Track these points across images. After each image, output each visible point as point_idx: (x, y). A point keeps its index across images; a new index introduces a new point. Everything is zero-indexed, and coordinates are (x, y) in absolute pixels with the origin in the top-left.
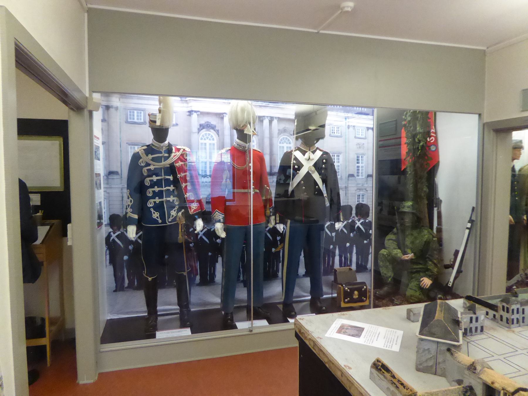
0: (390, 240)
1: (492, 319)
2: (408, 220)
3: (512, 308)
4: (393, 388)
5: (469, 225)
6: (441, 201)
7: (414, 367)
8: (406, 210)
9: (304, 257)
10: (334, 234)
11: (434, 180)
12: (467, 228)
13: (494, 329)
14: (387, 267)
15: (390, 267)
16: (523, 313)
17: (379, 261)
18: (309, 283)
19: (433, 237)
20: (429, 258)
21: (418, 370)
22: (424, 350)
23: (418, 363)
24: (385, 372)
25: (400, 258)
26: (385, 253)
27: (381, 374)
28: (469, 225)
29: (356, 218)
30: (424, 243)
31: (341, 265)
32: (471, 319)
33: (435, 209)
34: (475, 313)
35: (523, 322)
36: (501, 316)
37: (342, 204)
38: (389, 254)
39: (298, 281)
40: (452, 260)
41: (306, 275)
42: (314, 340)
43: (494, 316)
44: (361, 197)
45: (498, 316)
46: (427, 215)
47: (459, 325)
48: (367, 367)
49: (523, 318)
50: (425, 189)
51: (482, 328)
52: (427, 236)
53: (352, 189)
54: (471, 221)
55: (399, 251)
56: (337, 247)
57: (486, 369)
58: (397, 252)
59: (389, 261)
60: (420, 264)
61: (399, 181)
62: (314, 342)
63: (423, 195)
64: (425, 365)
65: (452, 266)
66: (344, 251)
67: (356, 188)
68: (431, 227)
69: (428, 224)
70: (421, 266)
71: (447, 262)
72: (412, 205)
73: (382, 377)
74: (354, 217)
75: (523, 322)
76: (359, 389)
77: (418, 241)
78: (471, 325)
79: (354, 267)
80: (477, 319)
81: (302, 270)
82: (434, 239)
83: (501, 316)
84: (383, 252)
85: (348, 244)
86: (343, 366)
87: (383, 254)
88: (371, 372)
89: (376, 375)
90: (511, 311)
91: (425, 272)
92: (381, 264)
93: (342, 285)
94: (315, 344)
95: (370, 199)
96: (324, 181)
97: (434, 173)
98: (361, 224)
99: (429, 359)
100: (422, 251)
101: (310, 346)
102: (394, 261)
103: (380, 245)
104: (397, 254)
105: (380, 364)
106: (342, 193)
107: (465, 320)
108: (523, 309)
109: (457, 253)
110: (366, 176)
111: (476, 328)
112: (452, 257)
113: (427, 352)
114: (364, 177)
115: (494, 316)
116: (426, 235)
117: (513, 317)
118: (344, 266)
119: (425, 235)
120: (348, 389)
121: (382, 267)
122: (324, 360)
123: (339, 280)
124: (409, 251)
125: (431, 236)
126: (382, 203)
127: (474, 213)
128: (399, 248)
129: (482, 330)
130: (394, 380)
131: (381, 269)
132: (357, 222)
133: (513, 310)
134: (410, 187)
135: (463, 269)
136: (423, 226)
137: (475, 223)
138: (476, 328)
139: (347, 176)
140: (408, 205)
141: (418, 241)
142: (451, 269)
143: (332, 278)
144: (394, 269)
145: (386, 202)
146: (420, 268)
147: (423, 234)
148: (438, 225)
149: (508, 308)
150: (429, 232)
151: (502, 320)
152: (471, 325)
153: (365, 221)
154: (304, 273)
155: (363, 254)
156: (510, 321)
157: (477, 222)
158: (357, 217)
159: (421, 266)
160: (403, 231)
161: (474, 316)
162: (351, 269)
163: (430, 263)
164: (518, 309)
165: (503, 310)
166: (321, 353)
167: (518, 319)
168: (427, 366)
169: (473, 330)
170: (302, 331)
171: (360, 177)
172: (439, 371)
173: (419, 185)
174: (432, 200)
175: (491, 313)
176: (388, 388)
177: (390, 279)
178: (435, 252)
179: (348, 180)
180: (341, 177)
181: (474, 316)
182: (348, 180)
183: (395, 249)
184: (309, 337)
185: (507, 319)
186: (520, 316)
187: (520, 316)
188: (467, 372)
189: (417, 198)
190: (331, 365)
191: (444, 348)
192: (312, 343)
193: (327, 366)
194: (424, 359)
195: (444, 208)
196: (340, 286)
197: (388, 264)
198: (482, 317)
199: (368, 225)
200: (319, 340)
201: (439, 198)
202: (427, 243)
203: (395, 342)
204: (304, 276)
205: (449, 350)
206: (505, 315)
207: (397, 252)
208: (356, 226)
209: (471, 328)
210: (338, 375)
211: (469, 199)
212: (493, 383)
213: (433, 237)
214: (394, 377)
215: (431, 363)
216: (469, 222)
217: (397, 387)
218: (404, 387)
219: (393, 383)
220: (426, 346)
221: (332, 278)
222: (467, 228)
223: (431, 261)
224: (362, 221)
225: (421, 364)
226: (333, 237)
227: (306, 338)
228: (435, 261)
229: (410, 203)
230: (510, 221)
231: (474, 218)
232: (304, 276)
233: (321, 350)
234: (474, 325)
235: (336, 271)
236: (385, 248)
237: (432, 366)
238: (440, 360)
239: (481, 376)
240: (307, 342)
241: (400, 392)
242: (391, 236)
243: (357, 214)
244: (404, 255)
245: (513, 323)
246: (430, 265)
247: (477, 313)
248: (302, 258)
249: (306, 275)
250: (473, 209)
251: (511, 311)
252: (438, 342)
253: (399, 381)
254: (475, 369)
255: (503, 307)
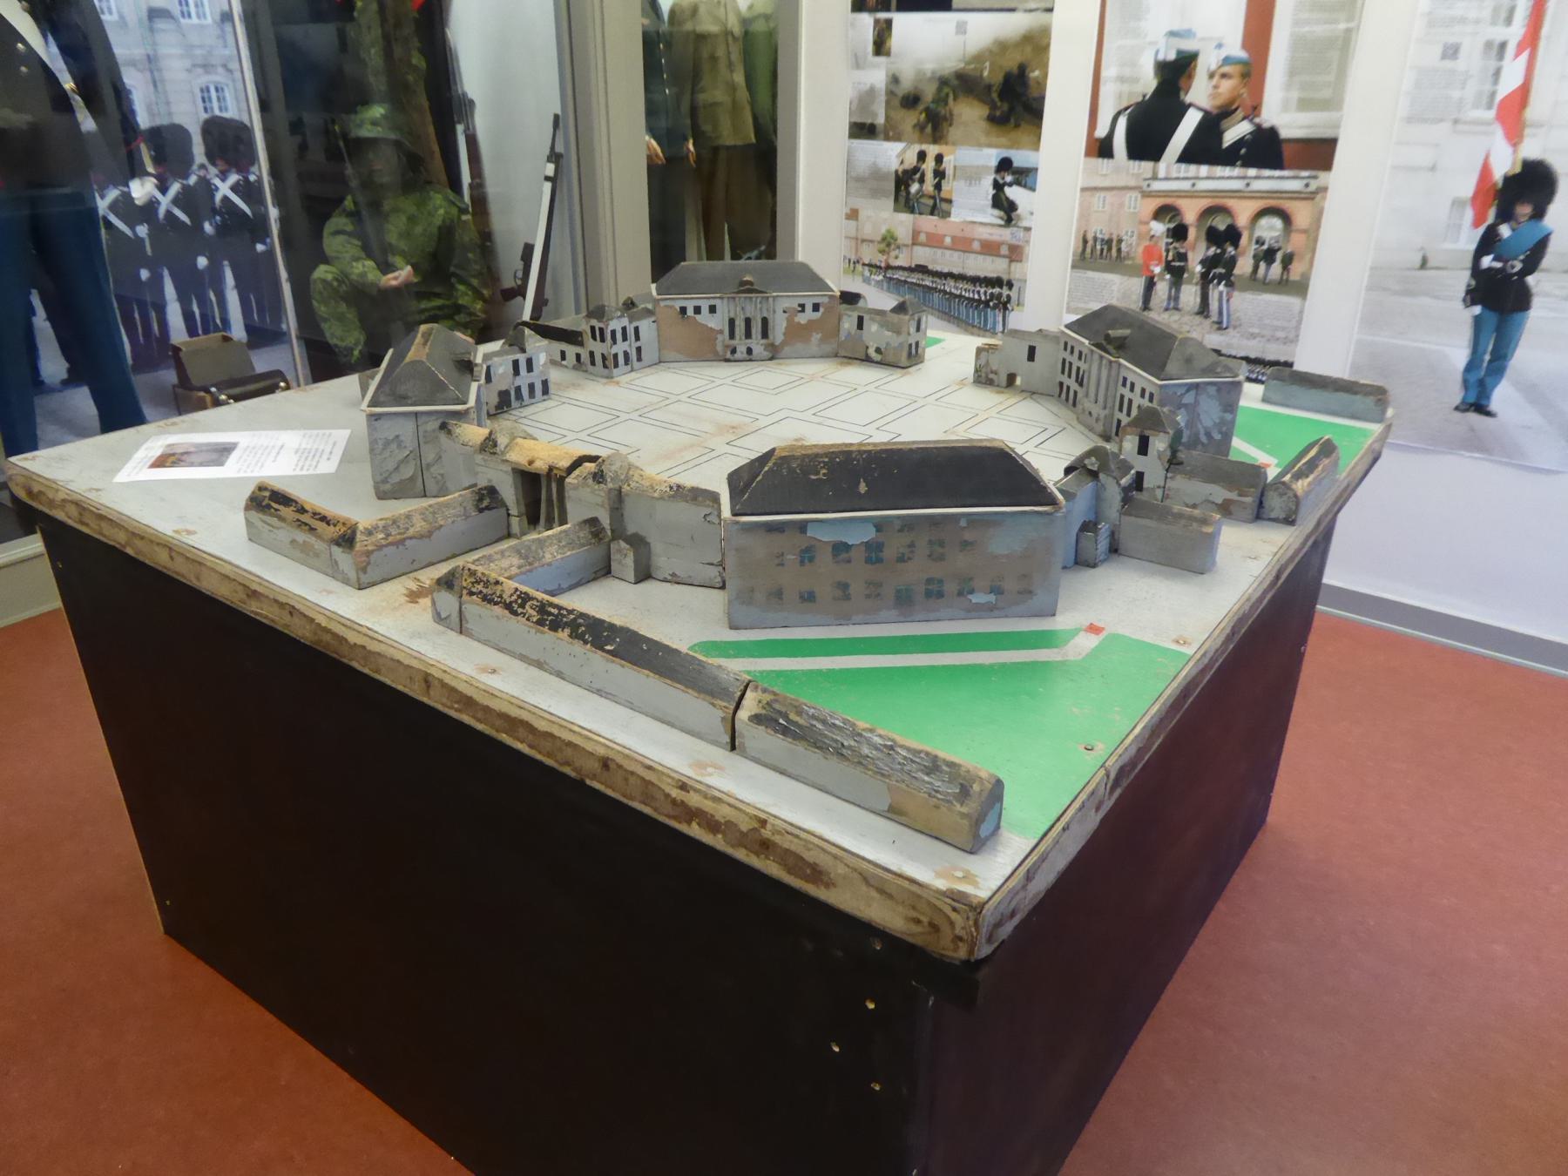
0: (338, 241)
1: (574, 368)
2: (385, 166)
3: (610, 328)
4: (302, 537)
5: (550, 169)
6: (472, 102)
7: (373, 491)
8: (367, 132)
9: (50, 318)
10: (142, 230)
11: (444, 34)
12: (547, 178)
13: (574, 385)
14: (341, 318)
15: (351, 315)
16: (637, 338)
17: (315, 304)
18: (91, 403)
19: (463, 211)
20: (454, 274)
21: (380, 498)
22: (387, 443)
23: (379, 478)
24: (280, 507)
25: (373, 284)
26: (329, 277)
27: (271, 515)
28: (550, 169)
29: (213, 171)
30: (435, 231)
31: (192, 331)
32: (516, 364)
33: (460, 128)
34: (523, 351)
35: (639, 359)
36: (592, 354)
37: (143, 121)
38: (343, 278)
39: (42, 404)
40: (520, 274)
41: (73, 379)
42: (75, 497)
43: (578, 356)
44: (213, 94)
45: (585, 357)
46: (436, 148)
47: (471, 371)
48: (237, 520)
49: (639, 350)
50: (418, 60)
51: (545, 383)
52: (441, 211)
53: (175, 68)
54: (555, 157)
55: (370, 263)
56: (166, 273)
57: (519, 440)
58: (365, 269)
59: (345, 298)
60: (438, 295)
61: (343, 43)
62: (77, 504)
63: (410, 78)
64: (396, 478)
65: (521, 291)
66: (191, 285)
67: (187, 63)
68: (455, 184)
69: (443, 177)
70: (438, 302)
71: (508, 282)
72: (384, 117)
73: (274, 521)
74: (202, 166)
75: (639, 359)
76: (218, 568)
77: (419, 229)
78: (518, 381)
79: (238, 332)
80: (529, 362)
81: (53, 365)
82: (464, 218)
83: (592, 354)
84: (322, 272)
85: (202, 262)
86: (170, 533)
87: (324, 281)
88: (249, 523)
89: (260, 524)
90: (608, 336)
91: (450, 317)
92: (321, 309)
93: (207, 391)
94: (80, 506)
95: (241, 103)
96: (67, 51)
97: (441, 12)
98: (234, 189)
99: (402, 462)
100: (434, 256)
101: (70, 522)
102: (362, 298)
103: (305, 249)
104: (363, 275)
105: (267, 494)
106: (133, 80)
107: (501, 371)
108: (637, 329)
109: (528, 250)
110: (218, 18)
111: (531, 387)
112: (520, 265)
113: (394, 446)
114: (209, 20)
115: (578, 356)
116: (439, 206)
117: (614, 350)
118: (206, 332)
119: (436, 209)
120: (194, 583)
121: (326, 320)
122: (117, 538)
123: (196, 375)
124: (398, 261)
125: (454, 211)
126: (300, 120)
127: (560, 134)
128: (370, 256)
129: (546, 391)
130: (305, 518)
131: (325, 326)
132: (217, 182)
133: (613, 333)
134: (374, 56)
135: (548, 293)
136: (429, 183)
137: (563, 162)
138: (531, 387)
139: (144, 14)
140: (373, 120)
141: (419, 229)
142: (519, 298)
143: (169, 376)
144: (363, 321)
145: (312, 119)
146: (440, 308)
147: (430, 207)
148: (473, 177)
149: (601, 330)
150: (446, 199)
151: (593, 363)
152: (518, 381)
153: (246, 180)
154: (65, 376)
155: (257, 285)
156: (610, 362)
157: (569, 163)
158: (214, 164)
159: (438, 302)
160: (376, 206)
161: (522, 358)
162: (227, 339)
163: (461, 287)
164: (624, 329)
165: (594, 338)
166: (103, 524)
167: (626, 354)
168: (401, 482)
169: (525, 392)
170: (35, 490)
171: (195, 20)
172: (431, 486)
173: (398, 51)
174: (445, 103)
175: (571, 350)
176: (293, 542)
177: (356, 353)
178: (470, 255)
179: (152, 30)
180: (122, 17)
181: (522, 358)
182: (152, 30)
183: (357, 259)
184: (61, 496)
185: (604, 358)
186: (628, 346)
187: (628, 346)
188: (479, 458)
189: (398, 95)
190: (138, 543)
191: (434, 425)
192: (73, 511)
193: (129, 551)
194: (391, 465)
195: (482, 121)
196: (202, 394)
197: (343, 307)
198: (541, 359)
199: (249, 191)
200: (92, 496)
201: (464, 94)
202: (447, 232)
203: (325, 457)
204: (67, 383)
205: (443, 426)
206: (598, 348)
207: (365, 269)
208: (218, 197)
209: (518, 389)
210: (160, 559)
211: (543, 95)
212: (531, 463)
213: (463, 211)
214: (302, 510)
215: (408, 471)
216: (549, 160)
217: (312, 529)
218: (328, 523)
219: (301, 524)
220: (388, 430)
221: (169, 376)
222: (547, 178)
223: (463, 281)
224: (234, 178)
225: (385, 481)
226: (142, 240)
227: (51, 503)
228: (475, 282)
229: (378, 111)
230: (650, 158)
231: (559, 149)
232: (67, 383)
233: (101, 517)
234: (524, 380)
235: (177, 350)
236: (326, 260)
237: (412, 479)
238: (429, 456)
239: (508, 457)
240: (59, 515)
241: (319, 537)
242: (338, 222)
243: (211, 156)
244: (385, 273)
245: (616, 366)
246: (464, 296)
247: (528, 348)
248: (41, 321)
249: (73, 379)
250: (556, 117)
251: (608, 336)
252: (416, 414)
253: (315, 514)
254: (495, 445)
255: (593, 328)
